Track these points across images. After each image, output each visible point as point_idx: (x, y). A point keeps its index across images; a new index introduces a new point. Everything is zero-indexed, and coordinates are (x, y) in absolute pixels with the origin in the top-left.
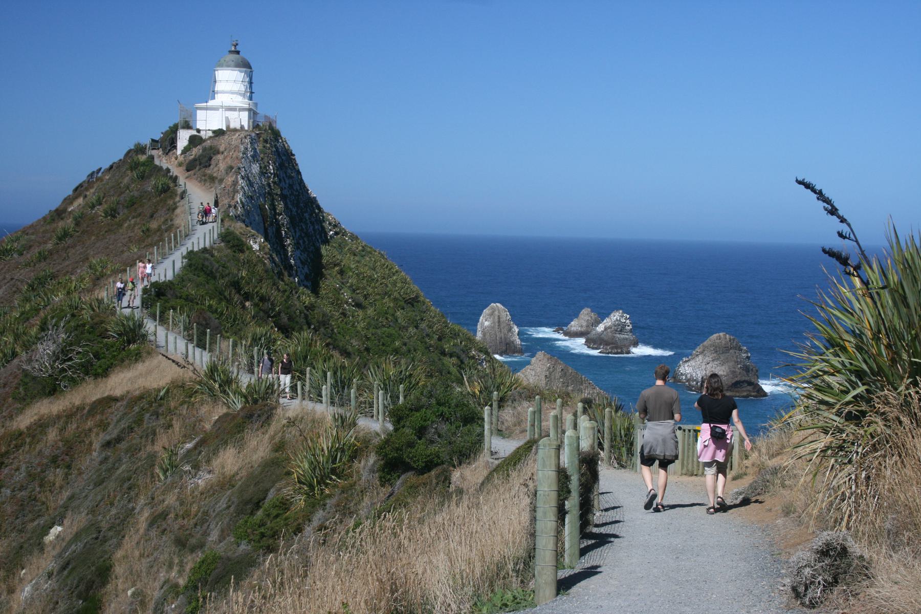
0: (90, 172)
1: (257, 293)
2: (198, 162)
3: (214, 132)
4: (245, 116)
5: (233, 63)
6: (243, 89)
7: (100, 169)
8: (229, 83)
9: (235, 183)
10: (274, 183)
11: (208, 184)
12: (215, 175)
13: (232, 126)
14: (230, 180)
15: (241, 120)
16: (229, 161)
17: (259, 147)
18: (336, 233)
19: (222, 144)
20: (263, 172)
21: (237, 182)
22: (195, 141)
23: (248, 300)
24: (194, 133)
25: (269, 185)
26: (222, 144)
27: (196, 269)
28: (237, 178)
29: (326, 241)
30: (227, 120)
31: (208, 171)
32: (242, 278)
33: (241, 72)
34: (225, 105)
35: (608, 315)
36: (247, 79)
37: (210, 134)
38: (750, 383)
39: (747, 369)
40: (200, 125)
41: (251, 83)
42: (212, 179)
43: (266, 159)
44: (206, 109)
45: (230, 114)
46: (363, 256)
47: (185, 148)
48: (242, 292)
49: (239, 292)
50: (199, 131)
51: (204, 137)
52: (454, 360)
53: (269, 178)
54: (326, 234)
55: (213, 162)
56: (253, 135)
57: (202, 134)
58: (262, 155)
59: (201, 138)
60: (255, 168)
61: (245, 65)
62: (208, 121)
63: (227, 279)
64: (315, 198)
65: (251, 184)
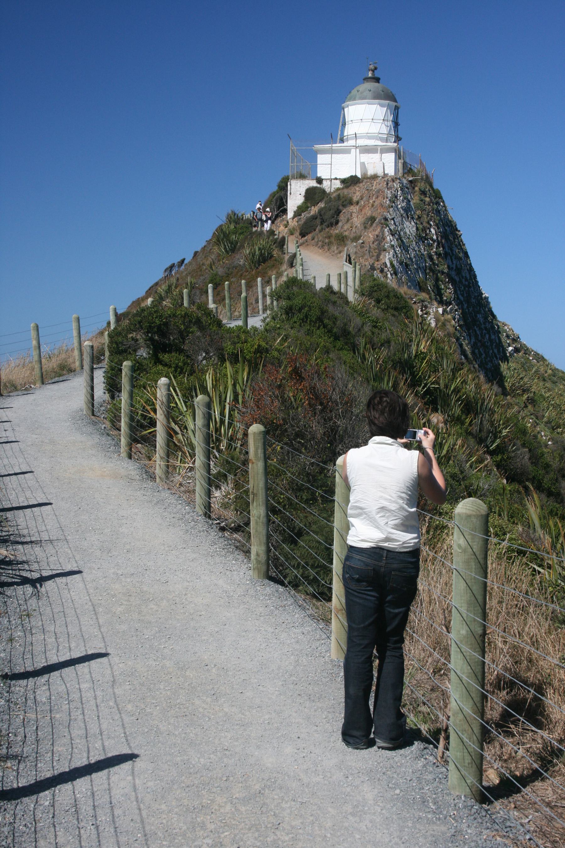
1: (457, 391)
2: (318, 221)
3: (343, 181)
4: (390, 158)
5: (370, 94)
6: (385, 130)
7: (183, 261)
8: (365, 118)
9: (380, 239)
10: (439, 255)
12: (346, 233)
13: (370, 172)
14: (370, 236)
15: (386, 164)
16: (368, 212)
17: (415, 200)
18: (517, 350)
19: (356, 193)
20: (422, 237)
21: (384, 239)
22: (312, 195)
23: (435, 410)
24: (314, 184)
25: (431, 258)
26: (356, 193)
27: (304, 320)
28: (383, 232)
29: (505, 359)
30: (363, 165)
31: (335, 231)
32: (420, 356)
33: (382, 106)
34: (361, 143)
36: (391, 118)
37: (338, 184)
40: (322, 172)
41: (396, 124)
43: (425, 219)
44: (332, 152)
45: (366, 158)
46: (554, 383)
47: (299, 208)
48: (421, 390)
49: (414, 383)
51: (328, 190)
53: (430, 246)
54: (504, 350)
55: (342, 217)
56: (405, 181)
57: (326, 185)
58: (419, 212)
59: (324, 191)
60: (410, 228)
61: (387, 96)
62: (334, 167)
63: (384, 352)
64: (486, 298)
65: (404, 247)
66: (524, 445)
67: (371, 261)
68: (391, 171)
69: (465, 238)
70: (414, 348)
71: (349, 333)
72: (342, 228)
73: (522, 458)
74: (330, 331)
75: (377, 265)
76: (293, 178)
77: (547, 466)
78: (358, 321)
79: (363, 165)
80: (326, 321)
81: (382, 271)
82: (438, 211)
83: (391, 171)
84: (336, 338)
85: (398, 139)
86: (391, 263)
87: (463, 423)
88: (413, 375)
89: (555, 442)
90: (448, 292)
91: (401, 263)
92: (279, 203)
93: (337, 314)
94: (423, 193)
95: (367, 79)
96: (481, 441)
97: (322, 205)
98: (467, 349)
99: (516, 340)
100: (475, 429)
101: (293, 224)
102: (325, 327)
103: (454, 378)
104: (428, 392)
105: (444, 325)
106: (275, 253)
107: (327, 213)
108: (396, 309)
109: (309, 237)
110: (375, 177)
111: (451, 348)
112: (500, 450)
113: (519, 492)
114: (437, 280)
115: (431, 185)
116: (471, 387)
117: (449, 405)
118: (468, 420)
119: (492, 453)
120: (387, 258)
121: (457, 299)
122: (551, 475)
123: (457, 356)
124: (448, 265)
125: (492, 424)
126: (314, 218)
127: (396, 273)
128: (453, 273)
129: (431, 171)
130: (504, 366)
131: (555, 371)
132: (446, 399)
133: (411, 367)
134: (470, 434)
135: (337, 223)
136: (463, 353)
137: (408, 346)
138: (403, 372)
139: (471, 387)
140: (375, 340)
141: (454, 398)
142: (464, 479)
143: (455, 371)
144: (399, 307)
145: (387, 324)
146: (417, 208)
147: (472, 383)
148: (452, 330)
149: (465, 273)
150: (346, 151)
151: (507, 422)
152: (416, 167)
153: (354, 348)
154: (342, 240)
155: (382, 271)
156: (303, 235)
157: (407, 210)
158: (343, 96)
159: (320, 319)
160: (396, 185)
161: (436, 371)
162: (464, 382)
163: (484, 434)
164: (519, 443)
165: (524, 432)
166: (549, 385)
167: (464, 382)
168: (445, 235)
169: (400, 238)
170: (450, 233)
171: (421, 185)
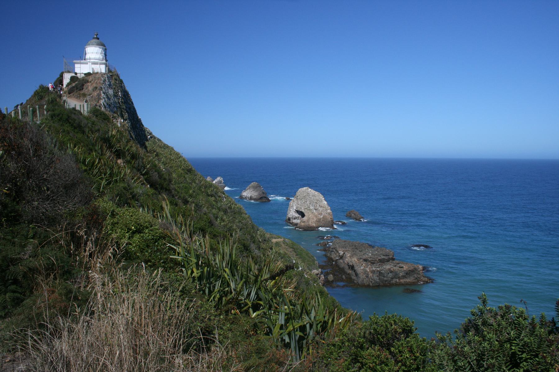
0: (16, 105)
1: (128, 150)
2: (75, 88)
3: (85, 74)
6: (101, 57)
8: (93, 52)
11: (82, 98)
13: (96, 71)
14: (95, 94)
15: (102, 69)
16: (95, 85)
17: (113, 82)
18: (151, 137)
20: (116, 95)
21: (101, 95)
22: (73, 79)
23: (120, 158)
24: (74, 75)
29: (147, 140)
30: (93, 69)
31: (82, 92)
32: (113, 136)
34: (92, 61)
35: (216, 178)
37: (83, 75)
38: (265, 197)
39: (263, 193)
40: (77, 70)
41: (106, 55)
42: (84, 95)
44: (81, 63)
45: (94, 66)
48: (114, 150)
50: (76, 74)
52: (213, 198)
53: (119, 99)
54: (147, 137)
55: (85, 87)
57: (78, 75)
59: (77, 78)
60: (111, 92)
61: (102, 45)
62: (81, 69)
65: (109, 99)
66: (156, 171)
67: (96, 103)
68: (103, 71)
69: (132, 97)
70: (110, 133)
71: (81, 126)
72: (85, 91)
73: (155, 176)
74: (72, 125)
75: (98, 104)
76: (65, 72)
77: (165, 179)
78: (86, 121)
79: (93, 69)
80: (70, 121)
81: (100, 107)
82: (122, 87)
83: (103, 71)
84: (75, 128)
85: (106, 61)
86: (104, 104)
87: (131, 163)
88: (110, 144)
89: (166, 170)
90: (126, 116)
91: (108, 104)
92: (60, 81)
93: (76, 118)
94: (116, 80)
95: (94, 38)
96: (139, 170)
97: (77, 83)
98: (134, 137)
99: (151, 134)
100: (136, 165)
101: (66, 89)
102: (70, 123)
103: (127, 145)
104: (117, 151)
105: (124, 126)
106: (58, 100)
107: (79, 85)
108: (104, 119)
109: (72, 94)
110: (97, 73)
111: (126, 134)
112: (146, 173)
113: (156, 194)
114: (122, 111)
115: (119, 77)
116: (134, 149)
117: (125, 156)
118: (133, 162)
119: (143, 175)
120: (102, 102)
121: (129, 118)
122: (167, 182)
123: (129, 137)
124: (126, 107)
125: (143, 163)
126: (73, 87)
127: (105, 107)
128: (128, 109)
129: (119, 73)
130: (147, 143)
131: (165, 144)
132: (124, 153)
133: (109, 141)
134: (134, 167)
135: (83, 89)
136: (131, 137)
137: (108, 132)
138: (104, 142)
139: (134, 149)
140: (93, 129)
141: (127, 153)
142: (130, 189)
143: (127, 142)
144: (105, 118)
145: (98, 123)
146: (114, 85)
147: (135, 147)
148: (127, 128)
149: (132, 110)
150: (87, 63)
151: (149, 162)
152: (113, 70)
153: (83, 132)
154: (84, 95)
155: (100, 107)
156: (69, 93)
157: (110, 85)
158: (86, 43)
159: (67, 120)
160: (106, 76)
161: (119, 142)
162: (131, 147)
163: (140, 168)
164: (154, 170)
165: (156, 166)
166: (163, 149)
167: (131, 147)
168: (124, 95)
169: (107, 95)
170: (126, 95)
171: (115, 77)
